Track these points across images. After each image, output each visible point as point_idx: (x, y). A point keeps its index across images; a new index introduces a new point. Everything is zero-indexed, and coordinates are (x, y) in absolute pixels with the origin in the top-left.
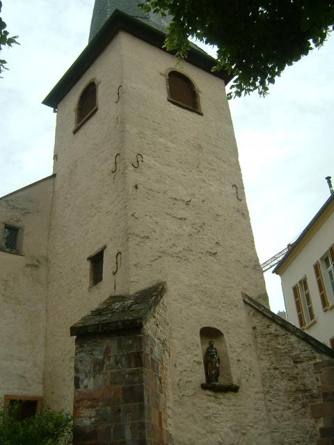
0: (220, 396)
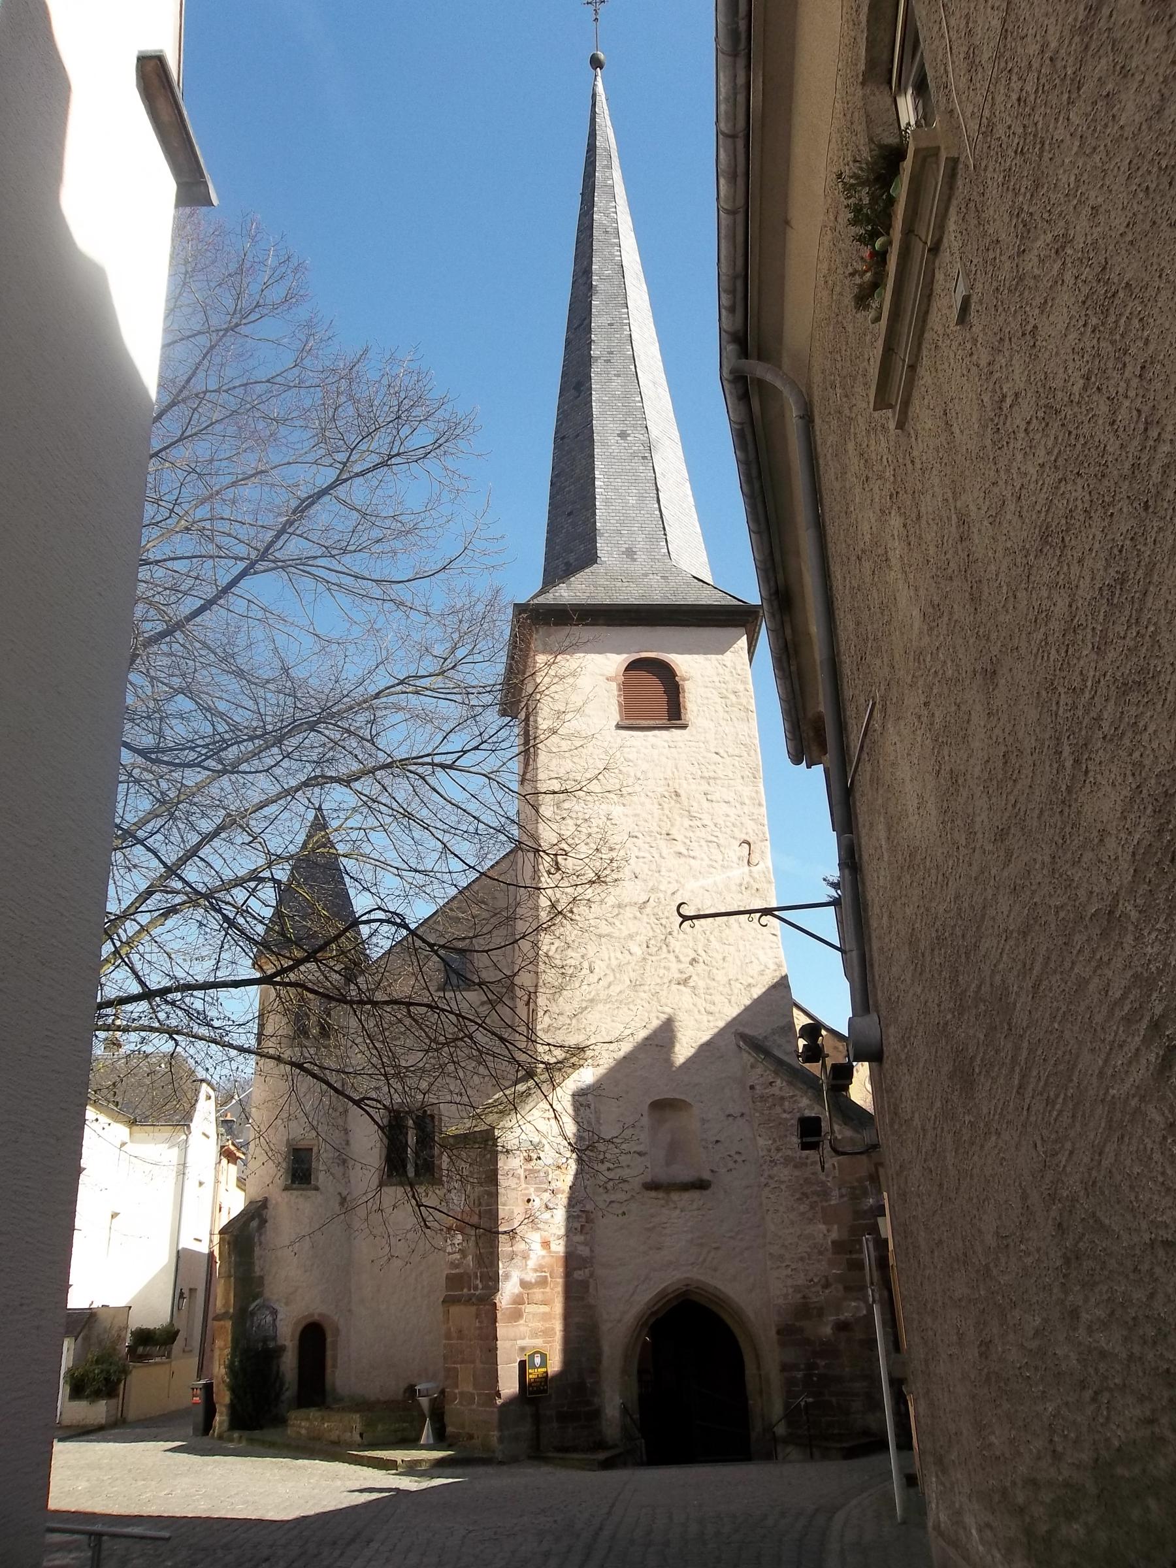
0: (675, 1196)
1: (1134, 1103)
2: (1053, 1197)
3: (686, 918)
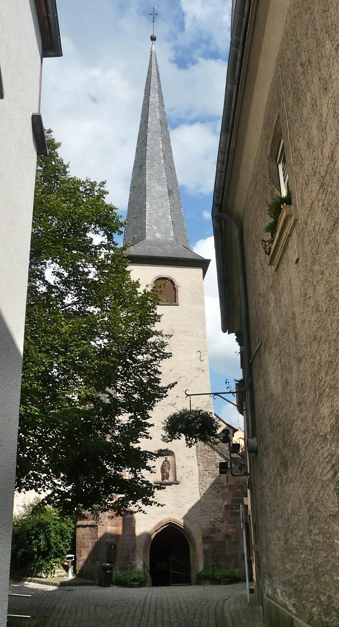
1: (328, 482)
2: (307, 502)
3: (188, 395)
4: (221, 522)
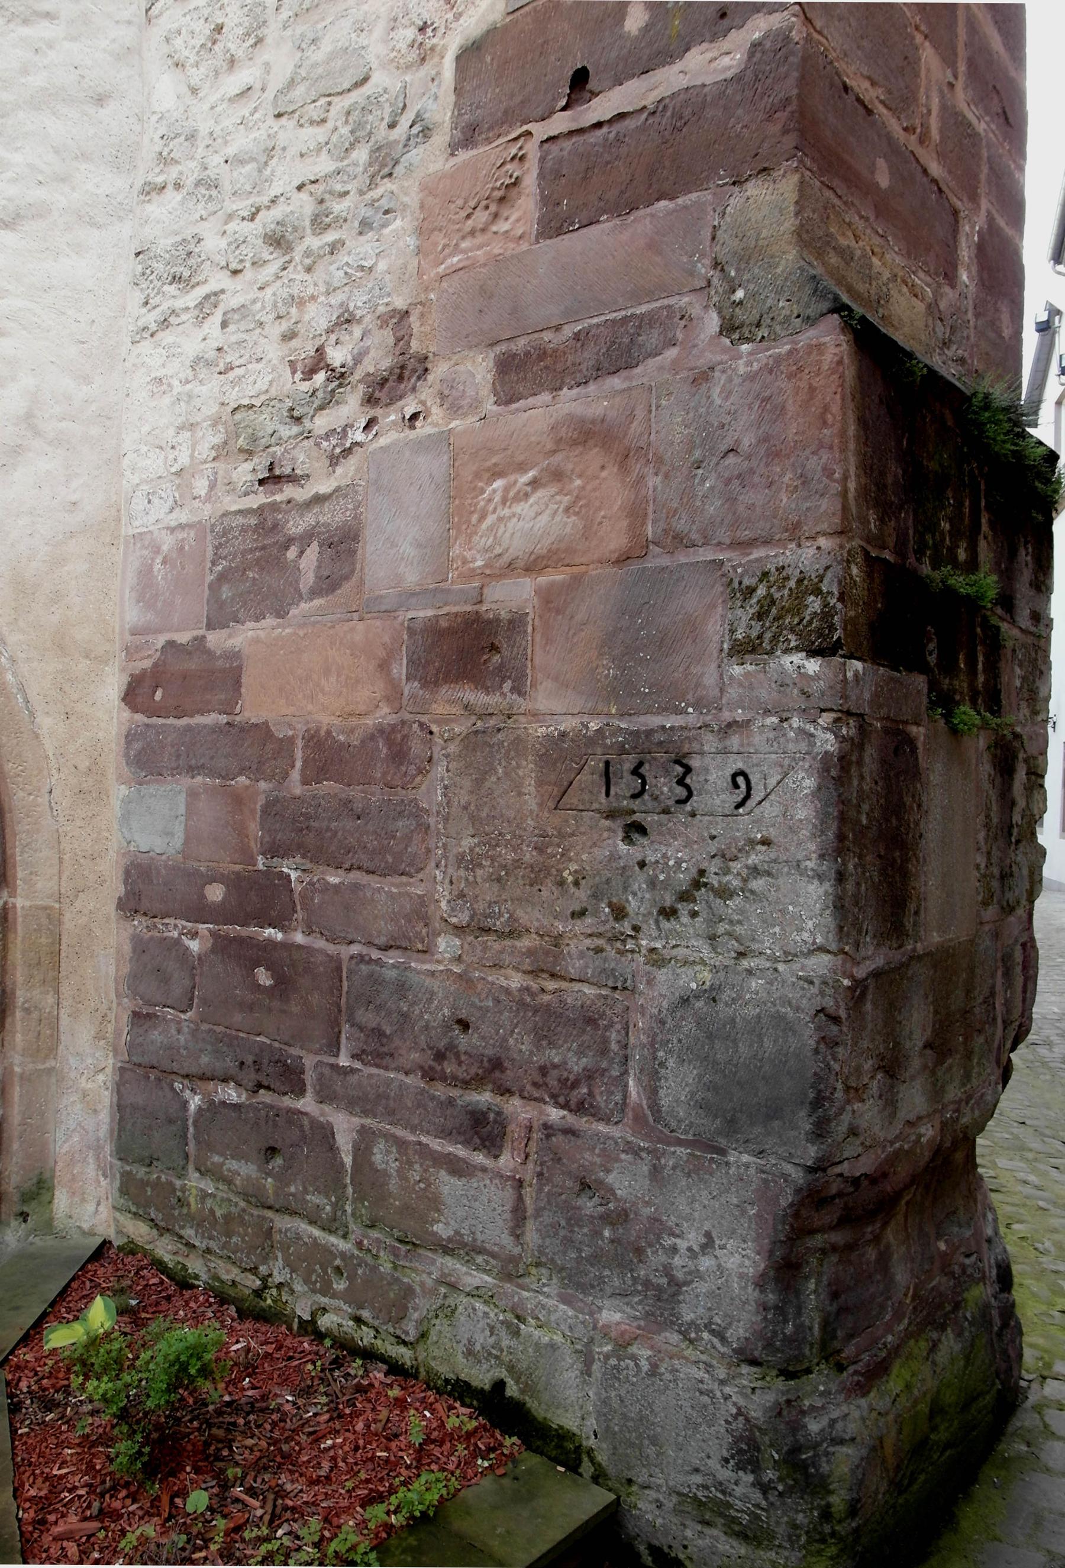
4: (383, 389)
